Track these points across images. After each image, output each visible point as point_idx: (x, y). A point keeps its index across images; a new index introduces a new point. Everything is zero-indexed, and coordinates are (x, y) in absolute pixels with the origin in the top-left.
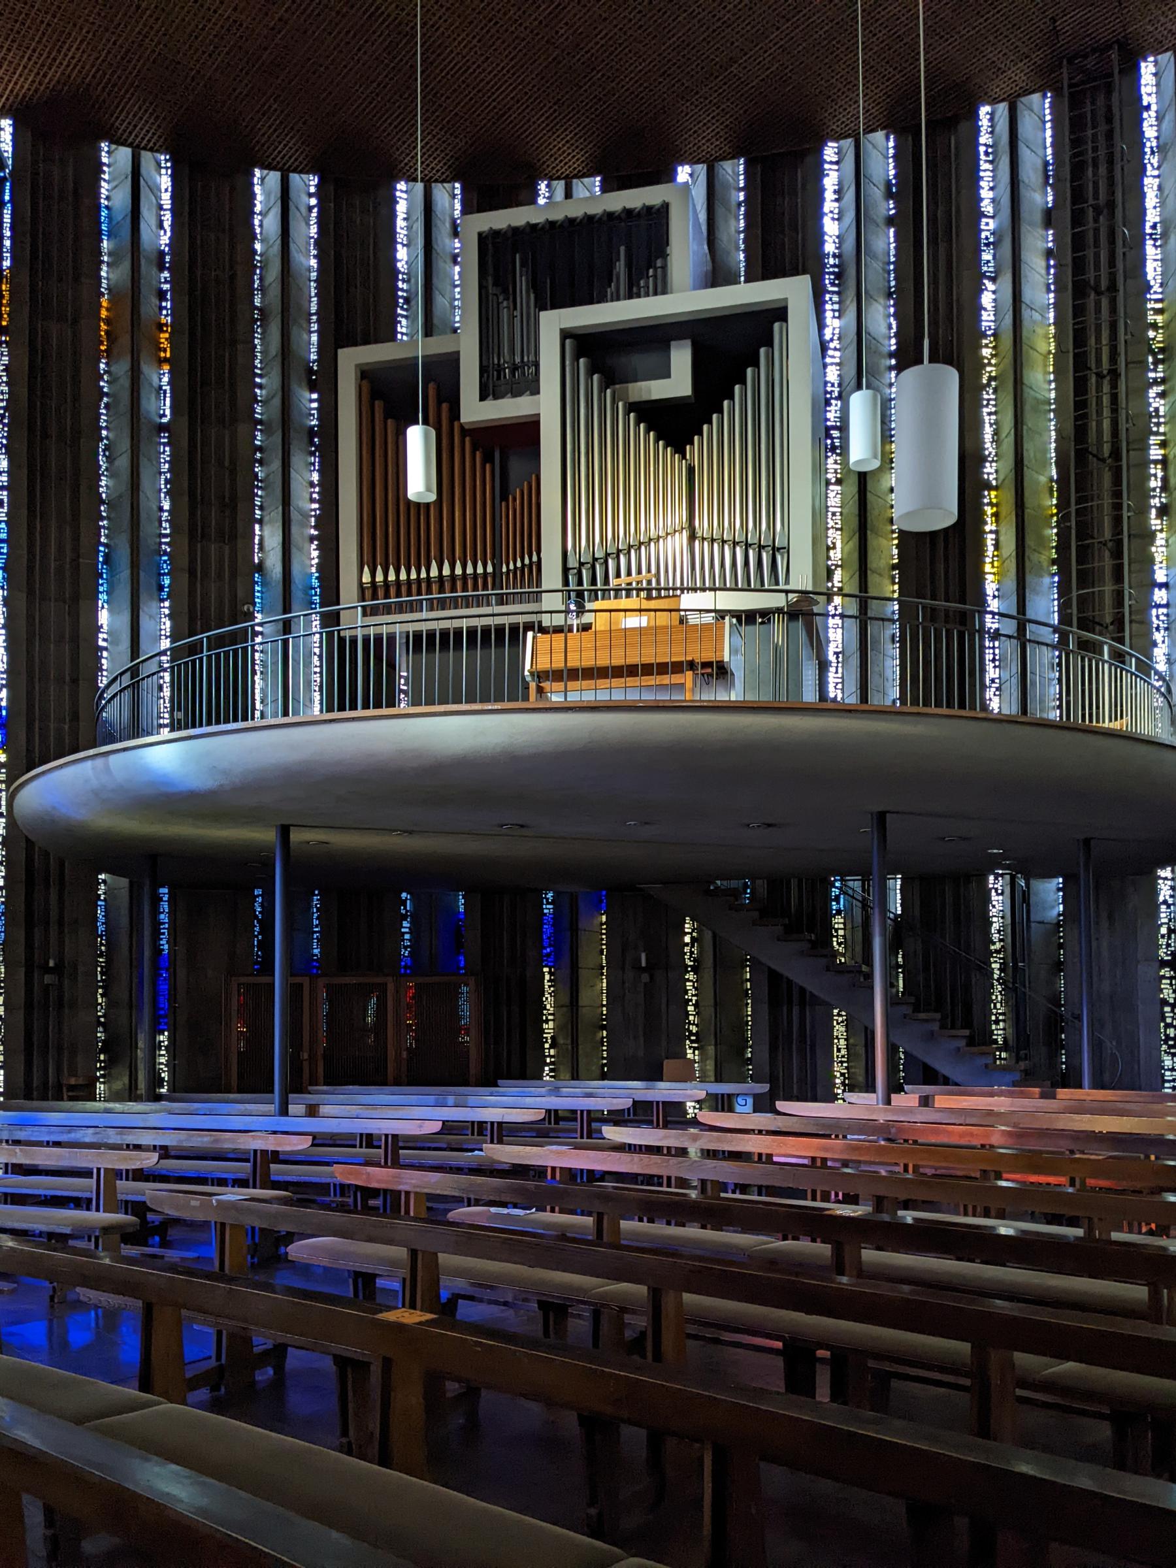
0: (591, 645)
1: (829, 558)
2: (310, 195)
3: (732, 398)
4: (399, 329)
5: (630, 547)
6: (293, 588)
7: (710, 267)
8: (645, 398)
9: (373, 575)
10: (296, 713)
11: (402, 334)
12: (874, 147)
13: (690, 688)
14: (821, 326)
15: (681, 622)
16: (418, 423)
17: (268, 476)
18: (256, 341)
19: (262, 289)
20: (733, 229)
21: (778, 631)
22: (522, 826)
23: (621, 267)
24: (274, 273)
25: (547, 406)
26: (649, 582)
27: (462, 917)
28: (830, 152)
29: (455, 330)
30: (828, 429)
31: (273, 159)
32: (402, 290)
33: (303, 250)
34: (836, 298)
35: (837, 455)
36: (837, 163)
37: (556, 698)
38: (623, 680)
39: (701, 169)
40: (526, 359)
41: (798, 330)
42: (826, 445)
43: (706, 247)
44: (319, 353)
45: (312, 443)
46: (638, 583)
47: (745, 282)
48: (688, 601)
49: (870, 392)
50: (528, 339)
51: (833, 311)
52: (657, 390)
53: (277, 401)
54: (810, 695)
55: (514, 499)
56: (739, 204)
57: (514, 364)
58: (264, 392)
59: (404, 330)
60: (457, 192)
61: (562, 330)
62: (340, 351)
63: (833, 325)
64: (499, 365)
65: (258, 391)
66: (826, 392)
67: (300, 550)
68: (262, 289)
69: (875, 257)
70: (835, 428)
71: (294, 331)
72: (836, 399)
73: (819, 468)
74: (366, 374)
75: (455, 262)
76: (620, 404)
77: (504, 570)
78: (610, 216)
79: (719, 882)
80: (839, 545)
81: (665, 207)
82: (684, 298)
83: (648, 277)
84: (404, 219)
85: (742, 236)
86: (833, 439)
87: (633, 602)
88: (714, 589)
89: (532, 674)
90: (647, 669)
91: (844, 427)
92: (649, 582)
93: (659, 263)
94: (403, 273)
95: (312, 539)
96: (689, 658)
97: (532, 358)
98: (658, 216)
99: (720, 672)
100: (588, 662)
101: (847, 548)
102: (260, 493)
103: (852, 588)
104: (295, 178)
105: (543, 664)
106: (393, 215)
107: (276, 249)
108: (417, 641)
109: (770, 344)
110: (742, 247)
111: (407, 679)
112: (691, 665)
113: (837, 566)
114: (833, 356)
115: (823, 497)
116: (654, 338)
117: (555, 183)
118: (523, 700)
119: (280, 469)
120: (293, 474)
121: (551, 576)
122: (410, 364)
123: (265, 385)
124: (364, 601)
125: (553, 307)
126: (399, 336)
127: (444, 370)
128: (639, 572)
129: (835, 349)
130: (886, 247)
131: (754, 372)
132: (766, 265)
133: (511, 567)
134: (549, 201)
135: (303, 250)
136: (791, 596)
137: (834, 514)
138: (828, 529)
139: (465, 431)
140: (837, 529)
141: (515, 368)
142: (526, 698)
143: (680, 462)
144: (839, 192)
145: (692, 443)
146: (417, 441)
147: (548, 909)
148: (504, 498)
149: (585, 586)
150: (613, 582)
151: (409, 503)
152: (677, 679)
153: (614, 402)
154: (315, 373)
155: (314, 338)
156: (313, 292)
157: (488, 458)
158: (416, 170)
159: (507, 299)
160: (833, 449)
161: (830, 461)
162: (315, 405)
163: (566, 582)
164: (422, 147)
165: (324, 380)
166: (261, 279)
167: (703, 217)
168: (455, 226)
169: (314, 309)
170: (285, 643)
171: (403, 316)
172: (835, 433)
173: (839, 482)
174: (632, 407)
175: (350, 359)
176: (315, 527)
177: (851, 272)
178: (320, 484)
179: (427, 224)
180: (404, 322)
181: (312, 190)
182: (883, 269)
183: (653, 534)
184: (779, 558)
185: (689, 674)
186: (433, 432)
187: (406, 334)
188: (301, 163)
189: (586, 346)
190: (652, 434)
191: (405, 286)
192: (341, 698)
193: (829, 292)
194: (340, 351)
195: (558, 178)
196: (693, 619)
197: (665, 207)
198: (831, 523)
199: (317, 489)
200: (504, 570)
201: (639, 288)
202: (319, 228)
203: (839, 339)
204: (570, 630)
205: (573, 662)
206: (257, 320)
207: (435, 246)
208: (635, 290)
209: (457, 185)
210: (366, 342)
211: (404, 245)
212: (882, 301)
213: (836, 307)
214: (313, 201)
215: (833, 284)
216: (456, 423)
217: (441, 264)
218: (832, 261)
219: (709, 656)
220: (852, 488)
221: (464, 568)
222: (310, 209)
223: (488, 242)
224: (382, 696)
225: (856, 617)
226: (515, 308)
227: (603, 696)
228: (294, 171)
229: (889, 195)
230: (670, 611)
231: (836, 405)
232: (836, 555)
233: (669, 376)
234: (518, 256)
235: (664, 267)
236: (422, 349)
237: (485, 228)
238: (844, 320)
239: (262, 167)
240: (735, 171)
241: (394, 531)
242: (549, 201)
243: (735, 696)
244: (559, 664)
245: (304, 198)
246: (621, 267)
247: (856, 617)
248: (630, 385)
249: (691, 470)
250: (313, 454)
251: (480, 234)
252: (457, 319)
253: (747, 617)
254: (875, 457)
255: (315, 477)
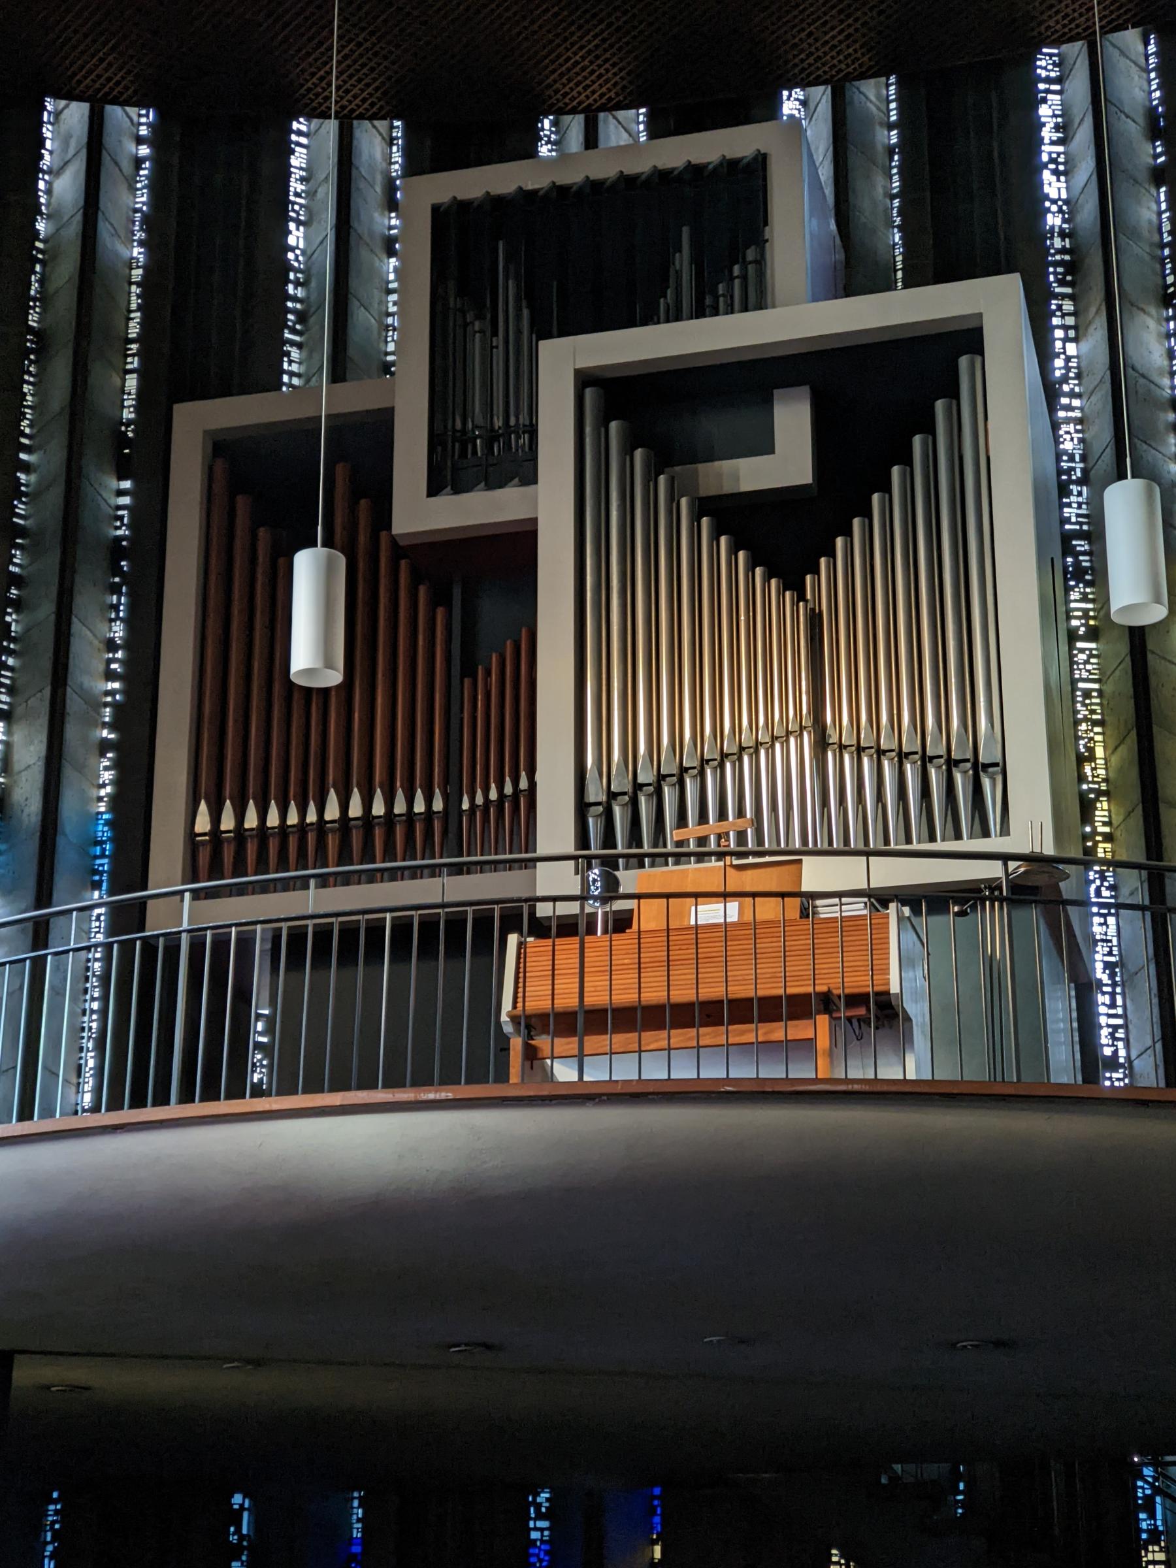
0: (630, 959)
1: (1082, 778)
2: (140, 141)
3: (886, 488)
4: (285, 366)
5: (704, 762)
6: (61, 842)
7: (841, 256)
8: (728, 489)
9: (216, 818)
10: (48, 1113)
11: (292, 374)
12: (1122, 53)
13: (824, 1055)
14: (1045, 355)
15: (804, 913)
16: (313, 544)
17: (27, 630)
18: (26, 388)
19: (44, 298)
20: (880, 190)
21: (993, 923)
22: (488, 1347)
23: (683, 261)
24: (67, 269)
25: (550, 505)
26: (741, 836)
27: (356, 1549)
28: (1045, 65)
29: (386, 368)
30: (1066, 539)
31: (79, 82)
32: (295, 299)
33: (122, 233)
34: (1068, 306)
35: (1088, 584)
36: (1059, 80)
37: (565, 1073)
38: (692, 1032)
39: (822, 95)
40: (512, 422)
41: (1006, 373)
42: (1065, 568)
43: (833, 226)
44: (138, 409)
45: (117, 571)
46: (719, 837)
47: (906, 286)
48: (817, 874)
49: (1139, 483)
50: (518, 352)
51: (1065, 328)
52: (751, 474)
53: (55, 497)
54: (1063, 1063)
55: (488, 673)
56: (891, 151)
57: (492, 430)
58: (33, 478)
59: (295, 368)
60: (397, 133)
61: (578, 373)
62: (176, 407)
63: (1068, 351)
64: (464, 431)
65: (22, 477)
66: (1060, 472)
67: (81, 769)
68: (44, 298)
69: (1135, 234)
70: (1080, 535)
71: (97, 370)
72: (1079, 482)
73: (1052, 610)
74: (222, 447)
75: (391, 253)
76: (684, 501)
77: (465, 806)
78: (663, 176)
79: (898, 1468)
80: (1099, 752)
81: (760, 162)
82: (798, 314)
83: (732, 279)
84: (302, 180)
85: (896, 203)
86: (1076, 555)
87: (707, 873)
88: (868, 854)
89: (515, 1019)
90: (740, 1011)
91: (1095, 533)
92: (741, 836)
93: (751, 254)
94: (296, 271)
95: (104, 747)
96: (822, 988)
97: (524, 419)
98: (750, 176)
99: (880, 1014)
100: (625, 996)
101: (1114, 760)
102: (11, 661)
103: (1133, 848)
104: (115, 113)
105: (538, 1000)
106: (285, 173)
107: (74, 230)
108: (299, 946)
109: (954, 394)
110: (898, 221)
111: (270, 1021)
112: (827, 1002)
113: (1100, 793)
114: (1072, 407)
115: (1065, 664)
116: (750, 381)
117: (567, 118)
118: (496, 1081)
119: (53, 617)
120: (76, 626)
121: (555, 827)
122: (306, 430)
123: (37, 465)
124: (195, 880)
125: (563, 333)
126: (286, 378)
127: (365, 443)
128: (722, 815)
129: (1072, 395)
130: (1154, 218)
131: (924, 444)
132: (937, 262)
133: (479, 800)
134: (556, 151)
135: (122, 233)
136: (1012, 865)
137: (1087, 694)
138: (1077, 723)
139: (399, 550)
140: (1095, 723)
141: (492, 437)
142: (502, 1076)
143: (795, 604)
144: (1065, 129)
145: (816, 571)
146: (311, 580)
147: (539, 1530)
148: (469, 671)
149: (620, 849)
150: (673, 834)
151: (290, 685)
152: (799, 1030)
153: (673, 500)
154: (128, 443)
155: (132, 382)
156: (134, 303)
157: (441, 598)
158: (328, 98)
159: (480, 317)
160: (1079, 574)
161: (1075, 596)
162: (126, 500)
163: (583, 840)
164: (339, 63)
165: (146, 458)
166: (41, 282)
167: (826, 172)
168: (390, 187)
169: (134, 330)
170: (38, 966)
171: (293, 343)
172: (1081, 545)
173: (1093, 634)
174: (704, 506)
175: (195, 422)
176: (112, 726)
177: (1095, 260)
178: (128, 645)
179: (347, 196)
180: (295, 354)
181: (143, 131)
182: (1153, 257)
183: (747, 739)
184: (986, 782)
185: (823, 1020)
186: (341, 560)
187: (298, 375)
188: (127, 88)
189: (614, 397)
190: (741, 555)
191: (300, 292)
192: (140, 1079)
193: (1057, 296)
194: (176, 407)
195: (574, 111)
196: (827, 910)
197: (760, 162)
198: (1083, 712)
199: (119, 655)
200: (465, 806)
201: (716, 298)
202: (150, 195)
203: (1078, 376)
204: (591, 930)
205: (597, 996)
206: (32, 351)
207: (354, 223)
208: (708, 301)
209: (397, 123)
210: (226, 392)
211: (299, 223)
212: (1153, 310)
213: (1070, 321)
214: (144, 150)
215: (1062, 283)
216: (383, 534)
217: (362, 255)
218: (1058, 243)
219: (858, 982)
220: (1123, 648)
221: (390, 802)
222: (138, 162)
223: (450, 223)
224: (216, 1076)
225: (1142, 908)
226: (495, 333)
227: (654, 1070)
228: (114, 102)
229: (1154, 132)
230: (783, 895)
231: (1078, 495)
232: (1096, 772)
233: (771, 451)
234: (501, 244)
235: (760, 262)
236: (326, 402)
237: (444, 198)
238: (1086, 346)
239: (57, 96)
240: (881, 97)
241: (257, 726)
242: (556, 151)
243: (913, 1066)
244: (567, 1000)
245: (132, 147)
246: (683, 261)
247: (1142, 908)
248: (701, 467)
249: (815, 620)
250: (115, 589)
251: (435, 209)
252: (391, 347)
253: (926, 901)
254: (1158, 601)
255: (118, 631)
